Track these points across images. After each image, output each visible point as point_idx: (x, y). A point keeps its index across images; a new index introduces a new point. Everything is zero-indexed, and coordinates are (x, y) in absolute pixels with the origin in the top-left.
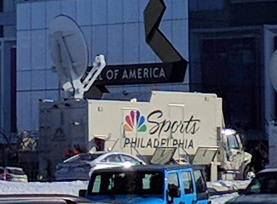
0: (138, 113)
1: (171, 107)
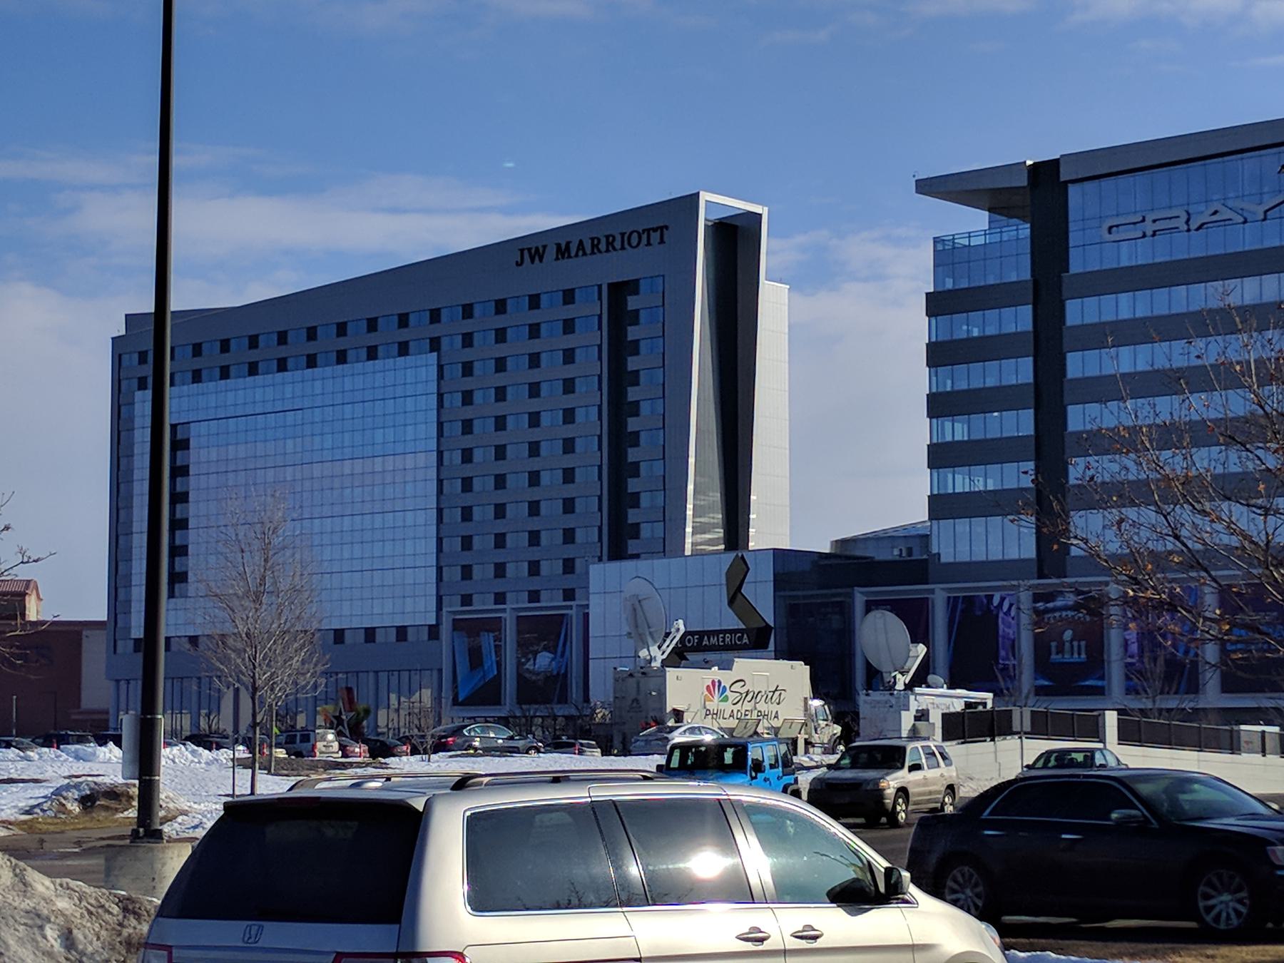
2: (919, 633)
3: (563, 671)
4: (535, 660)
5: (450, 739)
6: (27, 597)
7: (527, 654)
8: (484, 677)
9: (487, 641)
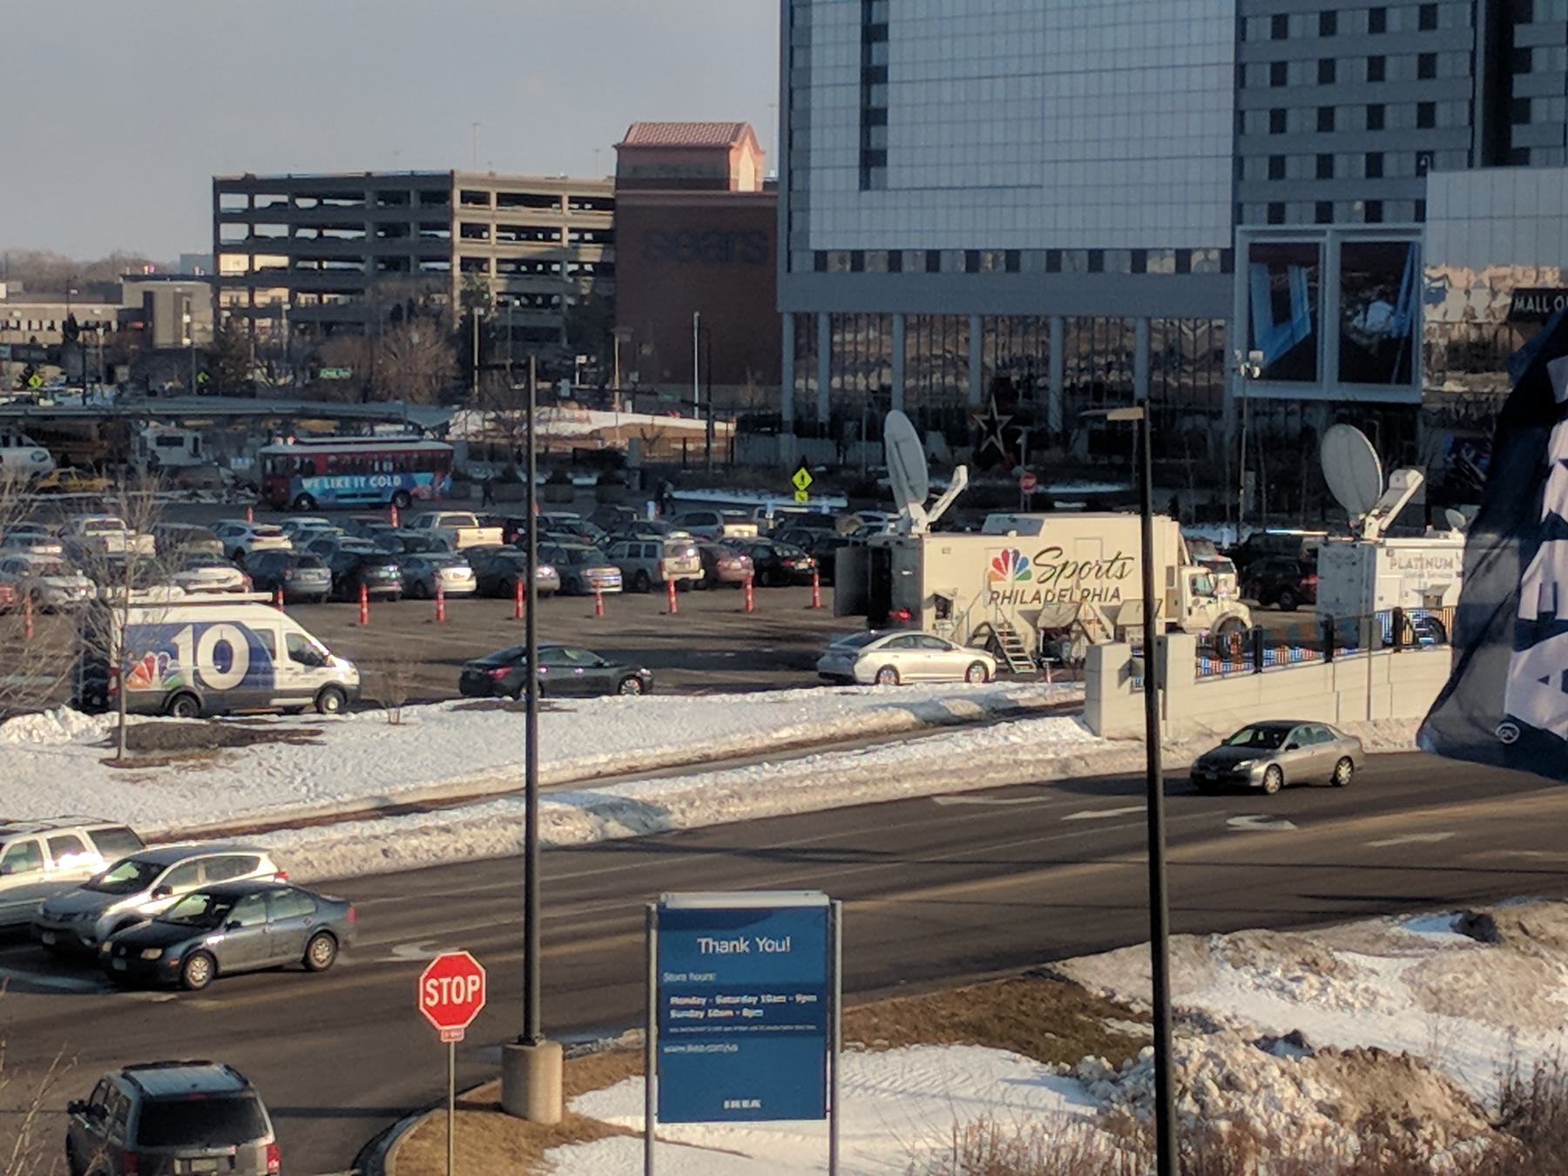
0: (1016, 553)
1: (520, 1007)
2: (1396, 455)
3: (1405, 334)
4: (1366, 313)
5: (499, 671)
6: (732, 153)
7: (1356, 303)
8: (1292, 336)
9: (1298, 280)
